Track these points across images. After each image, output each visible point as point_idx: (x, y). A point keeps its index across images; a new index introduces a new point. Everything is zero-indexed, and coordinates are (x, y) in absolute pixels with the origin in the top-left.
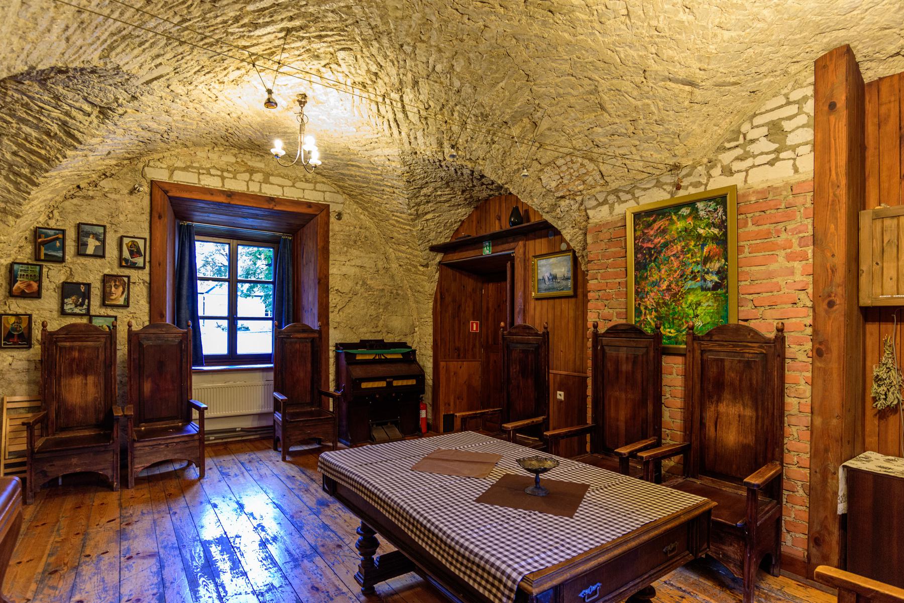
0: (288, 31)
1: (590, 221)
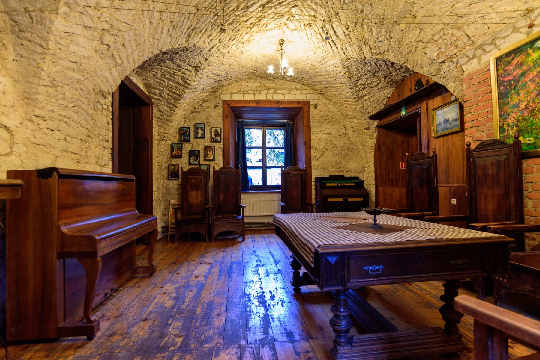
0: (264, 6)
1: (465, 73)
